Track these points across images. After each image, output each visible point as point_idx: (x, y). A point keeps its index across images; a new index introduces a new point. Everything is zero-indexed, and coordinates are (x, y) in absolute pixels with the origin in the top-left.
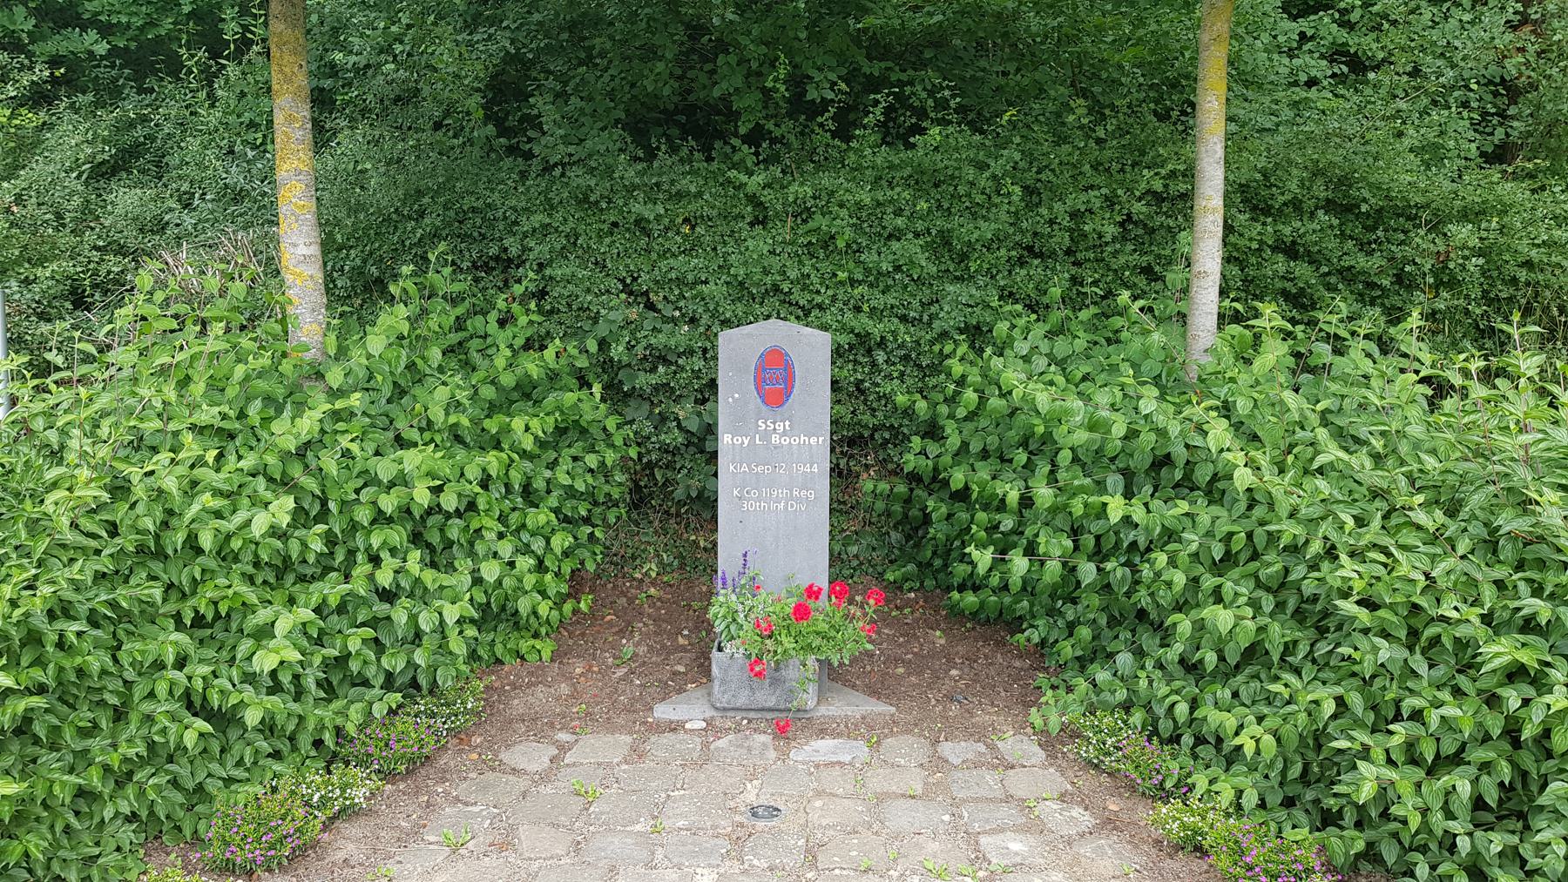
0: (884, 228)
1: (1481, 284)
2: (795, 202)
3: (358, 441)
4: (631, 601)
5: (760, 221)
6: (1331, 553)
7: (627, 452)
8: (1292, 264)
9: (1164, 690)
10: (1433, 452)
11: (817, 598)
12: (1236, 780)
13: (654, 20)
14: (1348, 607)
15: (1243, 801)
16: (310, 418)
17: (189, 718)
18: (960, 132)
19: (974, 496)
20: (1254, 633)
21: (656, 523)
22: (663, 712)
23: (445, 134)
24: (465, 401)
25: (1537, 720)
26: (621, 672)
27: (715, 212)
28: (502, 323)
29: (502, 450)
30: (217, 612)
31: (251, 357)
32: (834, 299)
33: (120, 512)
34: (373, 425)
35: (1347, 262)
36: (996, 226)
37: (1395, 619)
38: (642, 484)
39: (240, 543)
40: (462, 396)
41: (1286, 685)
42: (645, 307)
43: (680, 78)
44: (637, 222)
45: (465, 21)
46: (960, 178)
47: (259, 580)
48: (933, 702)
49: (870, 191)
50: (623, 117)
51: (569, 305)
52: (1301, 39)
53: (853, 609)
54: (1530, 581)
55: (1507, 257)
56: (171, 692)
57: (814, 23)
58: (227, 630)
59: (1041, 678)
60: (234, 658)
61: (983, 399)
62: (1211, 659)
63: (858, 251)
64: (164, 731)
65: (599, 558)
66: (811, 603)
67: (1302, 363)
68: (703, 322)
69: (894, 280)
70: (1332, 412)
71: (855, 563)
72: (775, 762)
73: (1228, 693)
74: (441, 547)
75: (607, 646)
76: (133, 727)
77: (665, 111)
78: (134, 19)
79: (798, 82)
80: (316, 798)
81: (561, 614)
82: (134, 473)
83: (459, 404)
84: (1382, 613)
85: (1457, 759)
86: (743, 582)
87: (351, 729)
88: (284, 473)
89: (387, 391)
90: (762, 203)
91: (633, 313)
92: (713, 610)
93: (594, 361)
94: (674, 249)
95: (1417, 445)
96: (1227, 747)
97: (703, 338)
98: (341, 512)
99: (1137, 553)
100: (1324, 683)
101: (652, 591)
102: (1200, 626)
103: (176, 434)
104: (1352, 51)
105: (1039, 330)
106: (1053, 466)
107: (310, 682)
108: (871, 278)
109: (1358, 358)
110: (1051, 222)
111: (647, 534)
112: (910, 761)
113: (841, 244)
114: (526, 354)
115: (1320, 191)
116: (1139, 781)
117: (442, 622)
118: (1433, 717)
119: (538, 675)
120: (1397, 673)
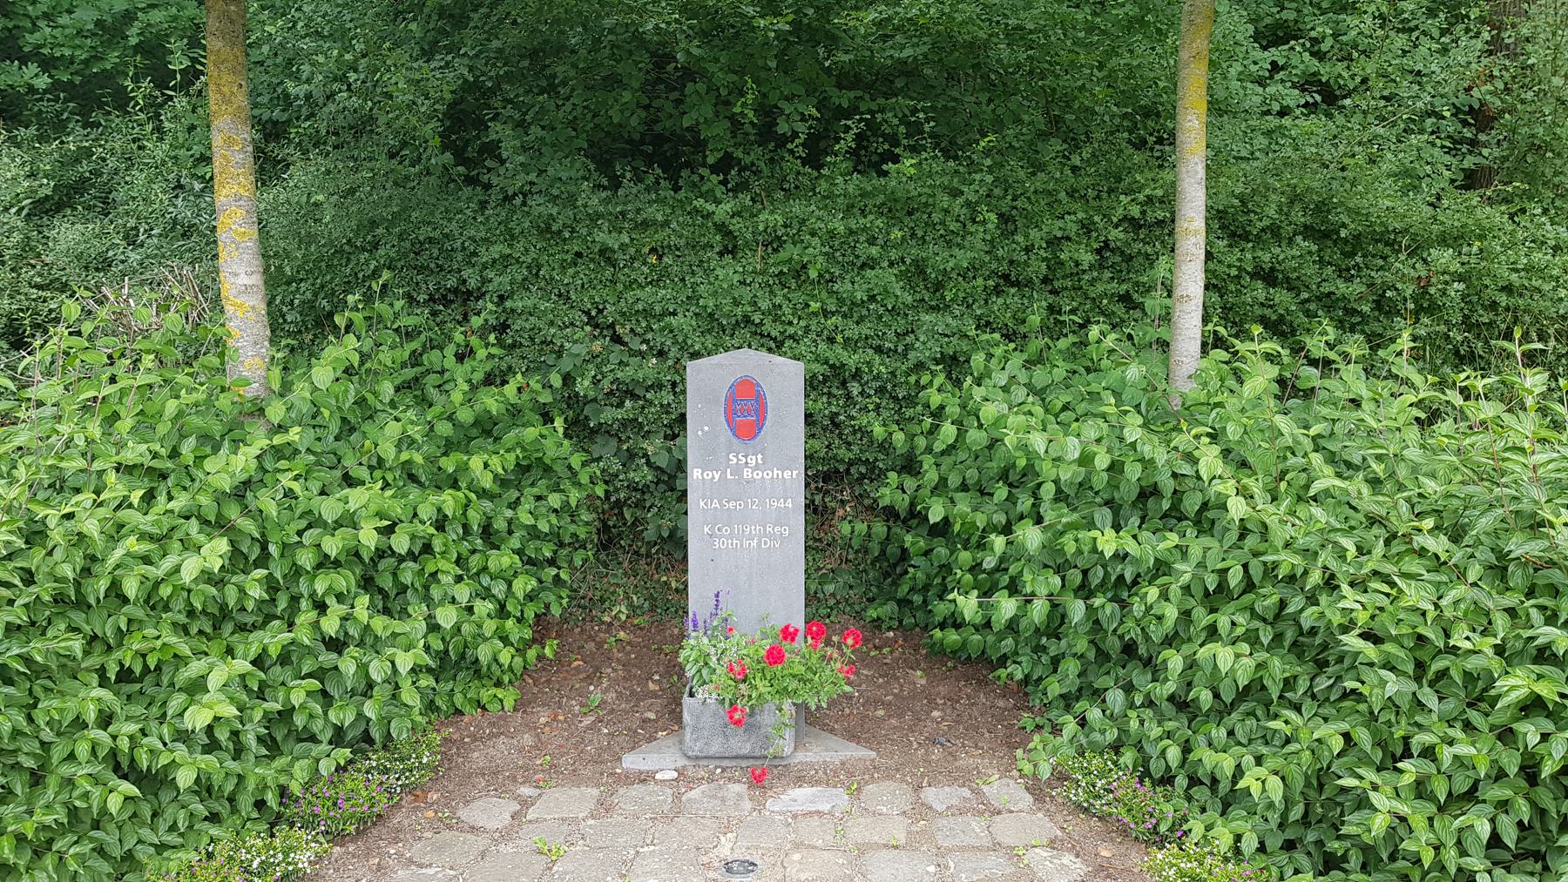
0: (857, 257)
1: (1462, 309)
2: (765, 231)
3: (302, 480)
4: (600, 645)
5: (730, 250)
6: (1330, 584)
7: (593, 489)
8: (1271, 290)
9: (1156, 732)
10: (1433, 476)
11: (793, 640)
12: (1234, 824)
13: (618, 47)
14: (1352, 641)
15: (1243, 845)
16: (245, 454)
17: (114, 781)
18: (933, 158)
19: (957, 528)
20: (1253, 669)
21: (626, 564)
22: (632, 761)
23: (400, 163)
24: (418, 437)
25: (1558, 757)
26: (588, 721)
27: (682, 242)
28: (460, 358)
29: (459, 489)
30: (145, 666)
31: (184, 391)
32: (807, 330)
33: (35, 559)
34: (318, 463)
35: (1326, 288)
36: (972, 255)
37: (1402, 654)
38: (611, 523)
39: (169, 590)
40: (416, 432)
41: (1286, 722)
42: (612, 340)
43: (647, 108)
44: (602, 252)
45: (423, 49)
46: (934, 205)
47: (194, 630)
48: (915, 745)
49: (842, 219)
50: (586, 146)
51: (532, 339)
52: (1273, 69)
53: (829, 650)
54: (1543, 608)
55: (1487, 282)
56: (94, 752)
57: (783, 52)
58: (158, 685)
59: (1027, 719)
60: (164, 715)
61: (961, 433)
62: (1206, 697)
63: (831, 281)
64: (86, 796)
65: (565, 602)
66: (786, 645)
67: (1286, 388)
68: (671, 354)
69: (868, 310)
70: (1323, 437)
71: (832, 602)
72: (750, 814)
73: (1223, 732)
74: (395, 592)
75: (573, 694)
76: (50, 794)
77: (630, 141)
78: (78, 53)
79: (769, 114)
80: (255, 864)
81: (525, 661)
82: (52, 516)
83: (413, 441)
84: (1389, 647)
85: (1471, 796)
86: (715, 624)
87: (295, 788)
88: (219, 515)
89: (334, 428)
90: (731, 232)
91: (597, 346)
92: (683, 654)
93: (559, 397)
94: (641, 280)
95: (1415, 469)
96: (1224, 787)
97: (672, 371)
98: (282, 555)
99: (1122, 589)
100: (1326, 720)
101: (622, 635)
102: (1191, 665)
103: (101, 473)
104: (1324, 80)
105: (1017, 360)
106: (1036, 499)
107: (250, 739)
108: (845, 309)
109: (1353, 380)
110: (1028, 250)
111: (615, 575)
112: (892, 808)
113: (813, 274)
114: (487, 388)
115: (1298, 217)
116: (1132, 826)
117: (395, 670)
118: (1446, 754)
119: (500, 726)
120: (1405, 707)
